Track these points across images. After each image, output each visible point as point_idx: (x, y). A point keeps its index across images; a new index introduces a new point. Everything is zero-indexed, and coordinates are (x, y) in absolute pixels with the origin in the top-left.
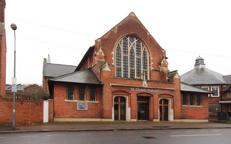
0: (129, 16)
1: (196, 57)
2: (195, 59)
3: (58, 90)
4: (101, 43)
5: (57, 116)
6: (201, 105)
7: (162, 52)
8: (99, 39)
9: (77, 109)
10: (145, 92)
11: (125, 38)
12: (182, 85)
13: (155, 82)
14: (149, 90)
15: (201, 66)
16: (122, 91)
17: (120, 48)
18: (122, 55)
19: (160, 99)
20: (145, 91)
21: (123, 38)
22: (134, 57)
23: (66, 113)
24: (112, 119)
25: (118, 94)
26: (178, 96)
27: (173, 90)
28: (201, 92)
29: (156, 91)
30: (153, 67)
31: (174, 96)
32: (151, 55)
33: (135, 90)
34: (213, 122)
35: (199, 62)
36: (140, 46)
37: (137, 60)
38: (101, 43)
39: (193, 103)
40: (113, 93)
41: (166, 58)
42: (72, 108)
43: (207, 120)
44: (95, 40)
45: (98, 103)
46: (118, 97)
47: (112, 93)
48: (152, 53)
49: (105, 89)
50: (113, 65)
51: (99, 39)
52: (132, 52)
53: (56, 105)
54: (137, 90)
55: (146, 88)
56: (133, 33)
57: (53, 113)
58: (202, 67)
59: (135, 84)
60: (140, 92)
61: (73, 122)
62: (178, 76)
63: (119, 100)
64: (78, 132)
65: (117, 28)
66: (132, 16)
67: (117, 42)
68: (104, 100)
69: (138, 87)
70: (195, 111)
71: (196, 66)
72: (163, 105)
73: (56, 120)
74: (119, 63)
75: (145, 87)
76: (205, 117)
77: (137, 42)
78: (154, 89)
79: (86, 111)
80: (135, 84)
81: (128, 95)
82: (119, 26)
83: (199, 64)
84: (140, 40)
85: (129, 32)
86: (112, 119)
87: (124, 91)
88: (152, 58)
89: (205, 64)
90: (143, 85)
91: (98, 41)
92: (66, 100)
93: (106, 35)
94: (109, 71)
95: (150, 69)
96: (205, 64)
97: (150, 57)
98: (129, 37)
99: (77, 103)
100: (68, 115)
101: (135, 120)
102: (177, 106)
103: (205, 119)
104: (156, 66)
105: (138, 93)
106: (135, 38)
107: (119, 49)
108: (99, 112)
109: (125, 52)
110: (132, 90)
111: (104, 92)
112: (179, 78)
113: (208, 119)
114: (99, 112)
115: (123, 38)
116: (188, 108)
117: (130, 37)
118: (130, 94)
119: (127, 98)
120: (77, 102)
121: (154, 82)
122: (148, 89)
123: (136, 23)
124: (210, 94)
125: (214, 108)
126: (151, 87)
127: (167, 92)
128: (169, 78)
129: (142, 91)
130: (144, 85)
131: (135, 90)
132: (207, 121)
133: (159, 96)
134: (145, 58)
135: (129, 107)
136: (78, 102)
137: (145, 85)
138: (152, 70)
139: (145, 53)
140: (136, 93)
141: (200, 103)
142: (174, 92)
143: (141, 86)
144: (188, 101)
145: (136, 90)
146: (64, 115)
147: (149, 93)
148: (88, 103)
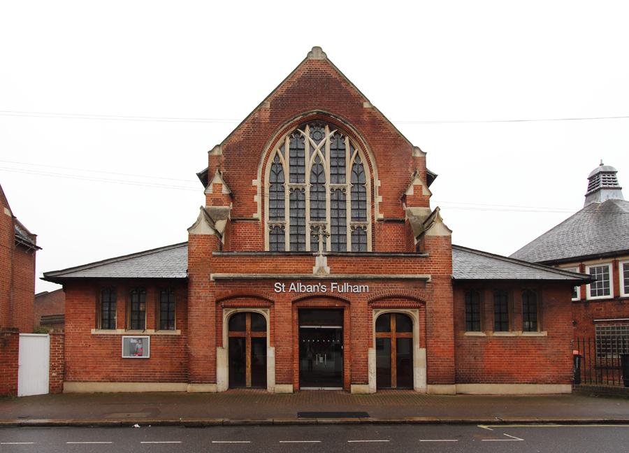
1: (592, 167)
2: (588, 174)
3: (76, 302)
4: (225, 159)
5: (71, 376)
6: (542, 330)
7: (414, 158)
8: (218, 149)
9: (123, 357)
10: (320, 294)
11: (296, 132)
12: (457, 259)
13: (356, 256)
14: (334, 285)
15: (603, 197)
16: (245, 293)
17: (281, 164)
18: (288, 183)
19: (378, 314)
20: (323, 289)
22: (324, 187)
23: (95, 367)
24: (215, 383)
25: (236, 304)
26: (443, 301)
29: (358, 288)
30: (381, 211)
31: (425, 299)
32: (375, 172)
33: (287, 288)
34: (589, 396)
35: (602, 180)
36: (345, 150)
37: (332, 194)
38: (225, 159)
39: (507, 322)
40: (220, 302)
41: (430, 178)
42: (110, 352)
44: (209, 152)
45: (179, 336)
46: (244, 314)
47: (218, 302)
48: (378, 166)
49: (195, 293)
50: (257, 220)
51: (218, 145)
52: (318, 172)
53: (69, 343)
54: (294, 289)
55: (323, 281)
56: (318, 113)
57: (61, 369)
58: (610, 198)
59: (290, 268)
61: (112, 393)
62: (443, 228)
63: (393, 325)
65: (268, 106)
66: (314, 59)
67: (271, 149)
68: (191, 324)
69: (298, 279)
71: (590, 197)
73: (70, 387)
74: (277, 213)
75: (321, 276)
76: (556, 374)
77: (332, 138)
78: (353, 281)
79: (146, 362)
80: (290, 268)
81: (419, 307)
82: (276, 99)
83: (601, 188)
84: (340, 131)
85: (304, 111)
86: (215, 383)
87: (254, 294)
88: (378, 183)
89: (621, 188)
90: (315, 269)
91: (216, 153)
92: (93, 331)
93: (236, 133)
94: (209, 236)
95: (373, 218)
96: (621, 188)
97: (372, 180)
98: (307, 127)
99: (123, 337)
100: (98, 373)
101: (289, 388)
103: (558, 383)
104: (390, 208)
105: (298, 297)
106: (327, 127)
107: (277, 168)
108: (181, 364)
109: (297, 175)
110: (278, 289)
111: (193, 299)
112: (447, 234)
114: (181, 364)
117: (311, 127)
118: (273, 302)
119: (416, 315)
120: (122, 335)
121: (354, 259)
122: (332, 284)
123: (329, 79)
124: (582, 283)
125: (614, 337)
126: (343, 276)
127: (400, 289)
129: (311, 289)
130: (318, 271)
131: (287, 288)
132: (567, 388)
134: (358, 185)
135: (421, 347)
136: (125, 335)
137: (321, 269)
138: (380, 220)
139: (358, 171)
140: (292, 299)
141: (535, 322)
142: (428, 286)
143: (308, 275)
144: (487, 315)
145: (291, 288)
146: (88, 373)
147: (337, 295)
148: (151, 336)
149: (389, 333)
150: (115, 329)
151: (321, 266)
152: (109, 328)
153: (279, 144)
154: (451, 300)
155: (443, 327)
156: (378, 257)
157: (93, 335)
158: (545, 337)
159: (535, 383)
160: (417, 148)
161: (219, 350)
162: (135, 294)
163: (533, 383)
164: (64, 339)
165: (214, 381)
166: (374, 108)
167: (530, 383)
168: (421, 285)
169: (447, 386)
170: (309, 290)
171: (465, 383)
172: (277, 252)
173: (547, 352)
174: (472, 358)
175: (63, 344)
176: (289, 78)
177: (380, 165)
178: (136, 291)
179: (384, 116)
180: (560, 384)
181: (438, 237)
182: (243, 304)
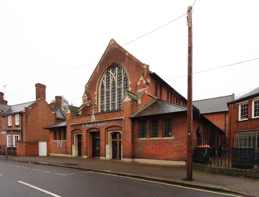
7: (143, 69)
20: (93, 126)
21: (105, 73)
27: (122, 119)
28: (179, 111)
35: (41, 89)
46: (117, 133)
47: (72, 132)
55: (94, 123)
56: (112, 63)
57: (49, 150)
60: (89, 128)
64: (49, 166)
72: (118, 140)
78: (101, 122)
91: (87, 86)
102: (126, 140)
103: (179, 160)
113: (186, 161)
116: (147, 142)
117: (112, 69)
127: (115, 123)
129: (90, 126)
133: (121, 129)
143: (90, 122)
149: (117, 139)
153: (102, 78)
155: (128, 137)
156: (108, 113)
158: (173, 139)
159: (167, 160)
160: (144, 64)
163: (166, 160)
166: (129, 54)
168: (120, 121)
171: (138, 158)
172: (103, 112)
173: (174, 146)
174: (141, 149)
179: (133, 56)
180: (179, 161)
181: (127, 102)
182: (77, 132)
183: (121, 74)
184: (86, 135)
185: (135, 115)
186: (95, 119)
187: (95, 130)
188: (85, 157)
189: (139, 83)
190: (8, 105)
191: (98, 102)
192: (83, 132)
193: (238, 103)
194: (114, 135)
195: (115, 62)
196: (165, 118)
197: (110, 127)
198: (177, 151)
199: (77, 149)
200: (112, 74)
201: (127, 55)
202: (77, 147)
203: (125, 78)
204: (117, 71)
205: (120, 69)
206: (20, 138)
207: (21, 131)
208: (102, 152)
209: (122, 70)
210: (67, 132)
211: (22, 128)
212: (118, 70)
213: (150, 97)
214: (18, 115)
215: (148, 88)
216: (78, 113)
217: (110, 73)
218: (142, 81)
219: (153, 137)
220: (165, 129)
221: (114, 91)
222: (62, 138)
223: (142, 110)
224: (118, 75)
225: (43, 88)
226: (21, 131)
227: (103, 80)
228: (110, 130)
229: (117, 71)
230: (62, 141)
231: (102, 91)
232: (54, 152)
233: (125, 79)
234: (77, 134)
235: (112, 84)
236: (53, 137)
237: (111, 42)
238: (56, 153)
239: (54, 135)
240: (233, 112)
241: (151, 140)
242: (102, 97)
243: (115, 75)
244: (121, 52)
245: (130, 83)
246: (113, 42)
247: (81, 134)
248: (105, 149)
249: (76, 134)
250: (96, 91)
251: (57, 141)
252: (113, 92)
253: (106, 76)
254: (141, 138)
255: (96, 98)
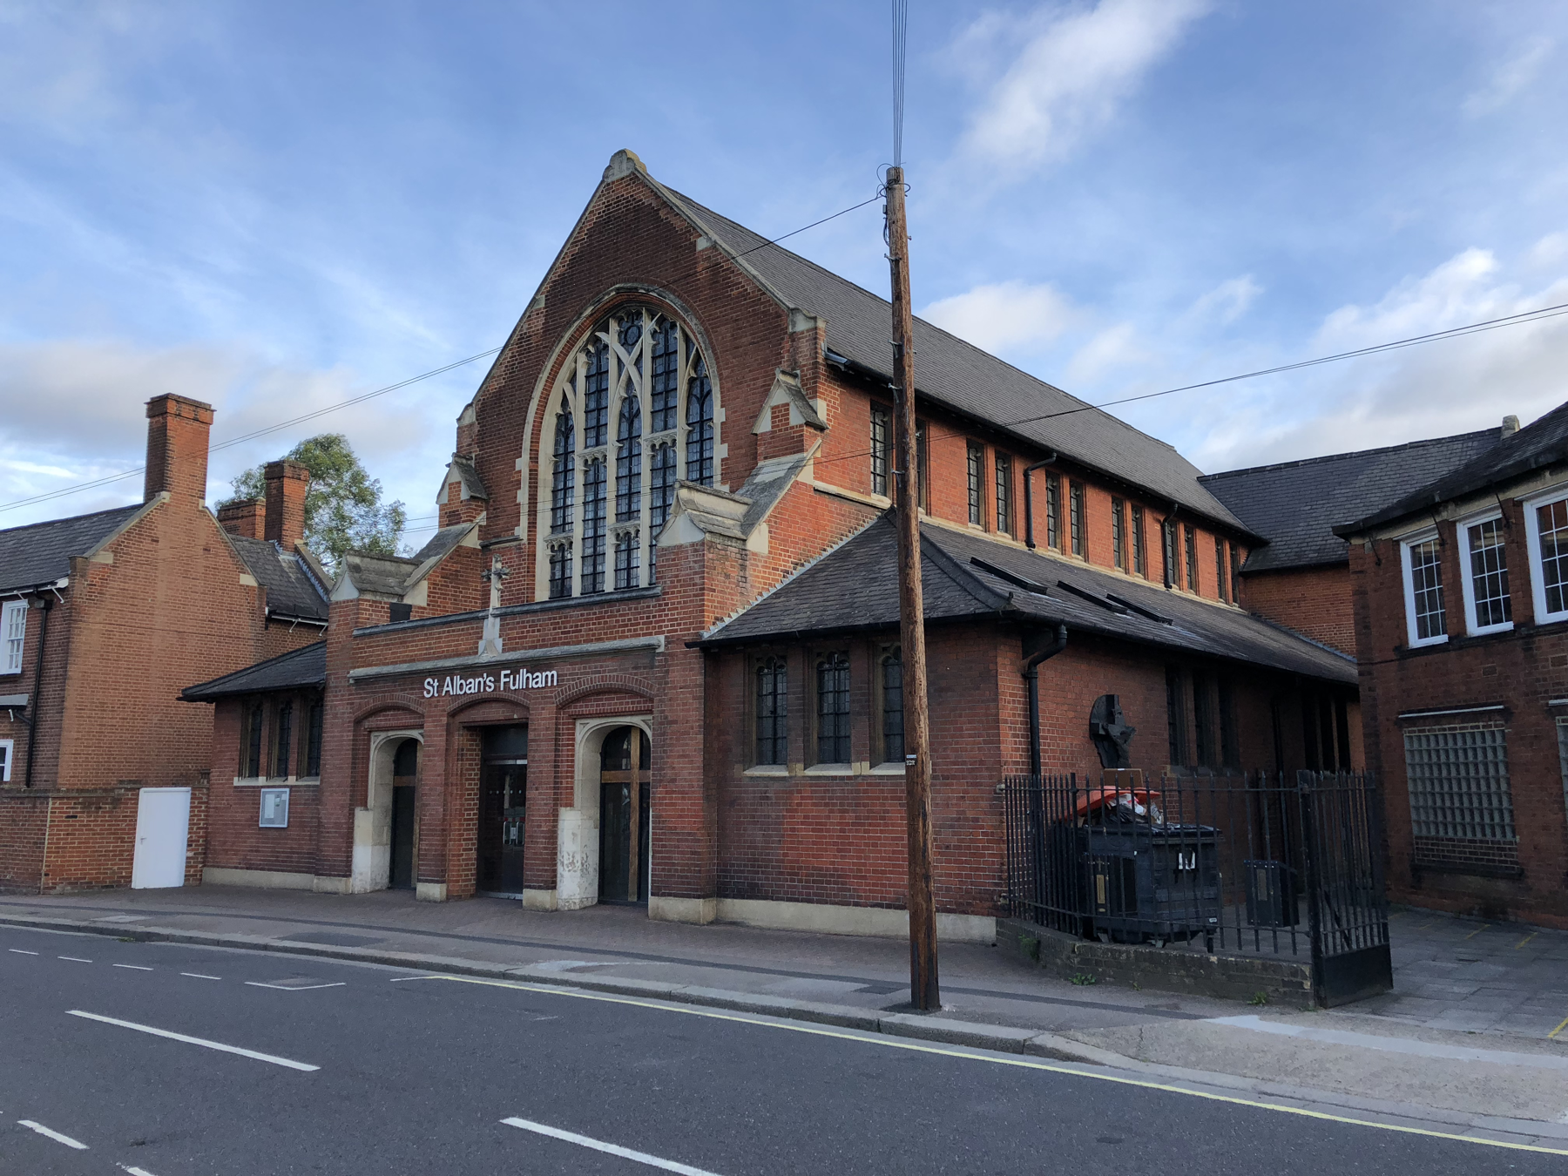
0: (606, 186)
7: (794, 337)
14: (506, 676)
21: (580, 343)
24: (554, 888)
27: (651, 648)
29: (540, 680)
37: (653, 457)
42: (248, 815)
43: (975, 921)
46: (625, 731)
47: (358, 722)
54: (450, 689)
55: (493, 668)
56: (618, 289)
60: (464, 700)
70: (850, 817)
78: (535, 665)
91: (467, 421)
92: (237, 782)
99: (263, 790)
105: (455, 705)
115: (580, 343)
117: (620, 321)
122: (503, 673)
127: (611, 674)
128: (361, 591)
129: (472, 686)
143: (470, 660)
150: (849, 762)
151: (491, 642)
152: (837, 760)
153: (564, 373)
154: (700, 692)
157: (236, 787)
161: (360, 814)
162: (829, 670)
164: (208, 795)
165: (347, 871)
167: (889, 907)
169: (891, 912)
170: (470, 689)
175: (207, 803)
176: (575, 235)
177: (725, 373)
178: (769, 668)
183: (672, 357)
184: (440, 741)
185: (727, 621)
186: (499, 643)
187: (495, 714)
188: (435, 891)
189: (764, 425)
190: (139, 882)
191: (532, 525)
192: (428, 726)
193: (1395, 534)
194: (612, 744)
195: (636, 288)
196: (885, 649)
197: (584, 696)
198: (947, 847)
199: (386, 836)
200: (622, 352)
201: (706, 249)
202: (389, 820)
203: (691, 381)
204: (647, 341)
205: (665, 326)
206: (15, 759)
207: (28, 713)
208: (533, 850)
209: (678, 334)
210: (328, 719)
211: (37, 696)
212: (654, 334)
213: (834, 505)
214: (23, 604)
215: (818, 455)
216: (402, 597)
217: (606, 347)
218: (780, 413)
219: (823, 760)
220: (886, 711)
221: (628, 456)
222: (292, 765)
223: (779, 586)
224: (654, 358)
225: (196, 420)
226: (28, 713)
227: (568, 388)
228: (585, 710)
229: (647, 341)
230: (292, 780)
231: (563, 456)
232: (236, 860)
233: (697, 391)
234: (390, 733)
235: (622, 415)
236: (236, 755)
237: (616, 166)
238: (250, 867)
239: (243, 738)
240: (1376, 591)
241: (811, 778)
242: (561, 491)
243: (638, 362)
244: (670, 227)
245: (719, 414)
246: (623, 171)
247: (415, 734)
248: (552, 836)
249: (383, 735)
250: (526, 455)
251: (262, 781)
252: (626, 462)
253: (589, 365)
254: (761, 763)
255: (523, 496)
